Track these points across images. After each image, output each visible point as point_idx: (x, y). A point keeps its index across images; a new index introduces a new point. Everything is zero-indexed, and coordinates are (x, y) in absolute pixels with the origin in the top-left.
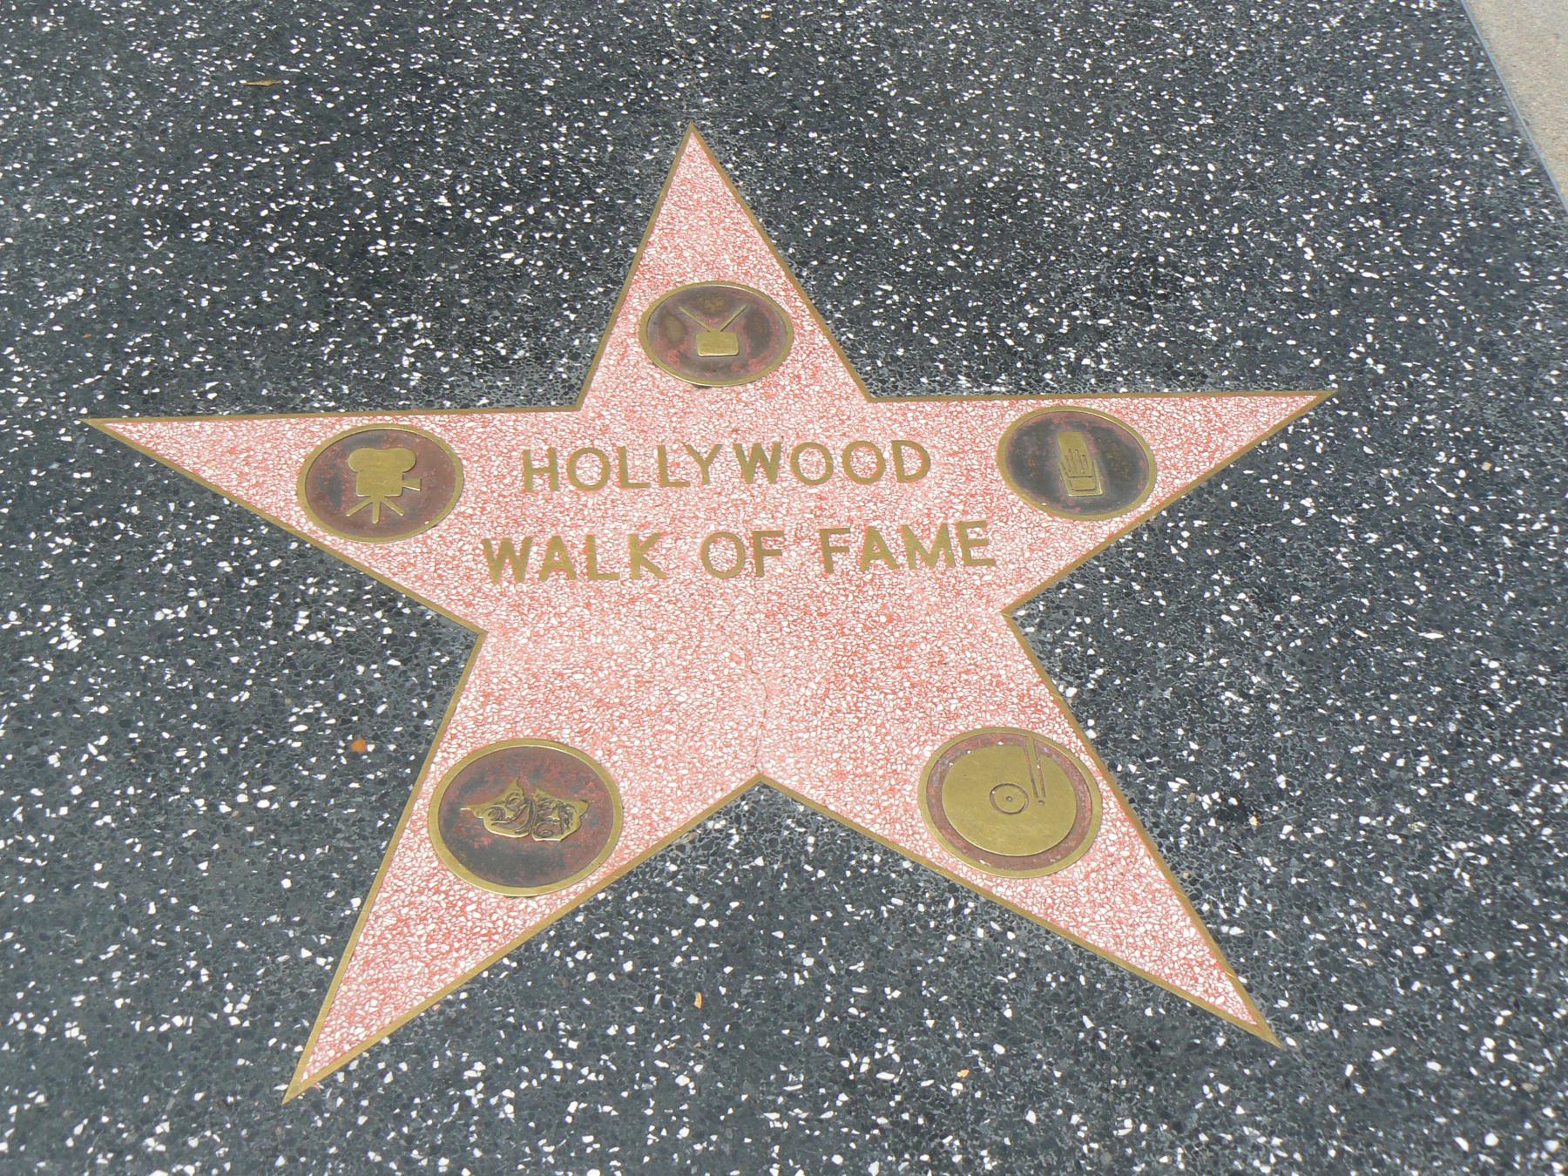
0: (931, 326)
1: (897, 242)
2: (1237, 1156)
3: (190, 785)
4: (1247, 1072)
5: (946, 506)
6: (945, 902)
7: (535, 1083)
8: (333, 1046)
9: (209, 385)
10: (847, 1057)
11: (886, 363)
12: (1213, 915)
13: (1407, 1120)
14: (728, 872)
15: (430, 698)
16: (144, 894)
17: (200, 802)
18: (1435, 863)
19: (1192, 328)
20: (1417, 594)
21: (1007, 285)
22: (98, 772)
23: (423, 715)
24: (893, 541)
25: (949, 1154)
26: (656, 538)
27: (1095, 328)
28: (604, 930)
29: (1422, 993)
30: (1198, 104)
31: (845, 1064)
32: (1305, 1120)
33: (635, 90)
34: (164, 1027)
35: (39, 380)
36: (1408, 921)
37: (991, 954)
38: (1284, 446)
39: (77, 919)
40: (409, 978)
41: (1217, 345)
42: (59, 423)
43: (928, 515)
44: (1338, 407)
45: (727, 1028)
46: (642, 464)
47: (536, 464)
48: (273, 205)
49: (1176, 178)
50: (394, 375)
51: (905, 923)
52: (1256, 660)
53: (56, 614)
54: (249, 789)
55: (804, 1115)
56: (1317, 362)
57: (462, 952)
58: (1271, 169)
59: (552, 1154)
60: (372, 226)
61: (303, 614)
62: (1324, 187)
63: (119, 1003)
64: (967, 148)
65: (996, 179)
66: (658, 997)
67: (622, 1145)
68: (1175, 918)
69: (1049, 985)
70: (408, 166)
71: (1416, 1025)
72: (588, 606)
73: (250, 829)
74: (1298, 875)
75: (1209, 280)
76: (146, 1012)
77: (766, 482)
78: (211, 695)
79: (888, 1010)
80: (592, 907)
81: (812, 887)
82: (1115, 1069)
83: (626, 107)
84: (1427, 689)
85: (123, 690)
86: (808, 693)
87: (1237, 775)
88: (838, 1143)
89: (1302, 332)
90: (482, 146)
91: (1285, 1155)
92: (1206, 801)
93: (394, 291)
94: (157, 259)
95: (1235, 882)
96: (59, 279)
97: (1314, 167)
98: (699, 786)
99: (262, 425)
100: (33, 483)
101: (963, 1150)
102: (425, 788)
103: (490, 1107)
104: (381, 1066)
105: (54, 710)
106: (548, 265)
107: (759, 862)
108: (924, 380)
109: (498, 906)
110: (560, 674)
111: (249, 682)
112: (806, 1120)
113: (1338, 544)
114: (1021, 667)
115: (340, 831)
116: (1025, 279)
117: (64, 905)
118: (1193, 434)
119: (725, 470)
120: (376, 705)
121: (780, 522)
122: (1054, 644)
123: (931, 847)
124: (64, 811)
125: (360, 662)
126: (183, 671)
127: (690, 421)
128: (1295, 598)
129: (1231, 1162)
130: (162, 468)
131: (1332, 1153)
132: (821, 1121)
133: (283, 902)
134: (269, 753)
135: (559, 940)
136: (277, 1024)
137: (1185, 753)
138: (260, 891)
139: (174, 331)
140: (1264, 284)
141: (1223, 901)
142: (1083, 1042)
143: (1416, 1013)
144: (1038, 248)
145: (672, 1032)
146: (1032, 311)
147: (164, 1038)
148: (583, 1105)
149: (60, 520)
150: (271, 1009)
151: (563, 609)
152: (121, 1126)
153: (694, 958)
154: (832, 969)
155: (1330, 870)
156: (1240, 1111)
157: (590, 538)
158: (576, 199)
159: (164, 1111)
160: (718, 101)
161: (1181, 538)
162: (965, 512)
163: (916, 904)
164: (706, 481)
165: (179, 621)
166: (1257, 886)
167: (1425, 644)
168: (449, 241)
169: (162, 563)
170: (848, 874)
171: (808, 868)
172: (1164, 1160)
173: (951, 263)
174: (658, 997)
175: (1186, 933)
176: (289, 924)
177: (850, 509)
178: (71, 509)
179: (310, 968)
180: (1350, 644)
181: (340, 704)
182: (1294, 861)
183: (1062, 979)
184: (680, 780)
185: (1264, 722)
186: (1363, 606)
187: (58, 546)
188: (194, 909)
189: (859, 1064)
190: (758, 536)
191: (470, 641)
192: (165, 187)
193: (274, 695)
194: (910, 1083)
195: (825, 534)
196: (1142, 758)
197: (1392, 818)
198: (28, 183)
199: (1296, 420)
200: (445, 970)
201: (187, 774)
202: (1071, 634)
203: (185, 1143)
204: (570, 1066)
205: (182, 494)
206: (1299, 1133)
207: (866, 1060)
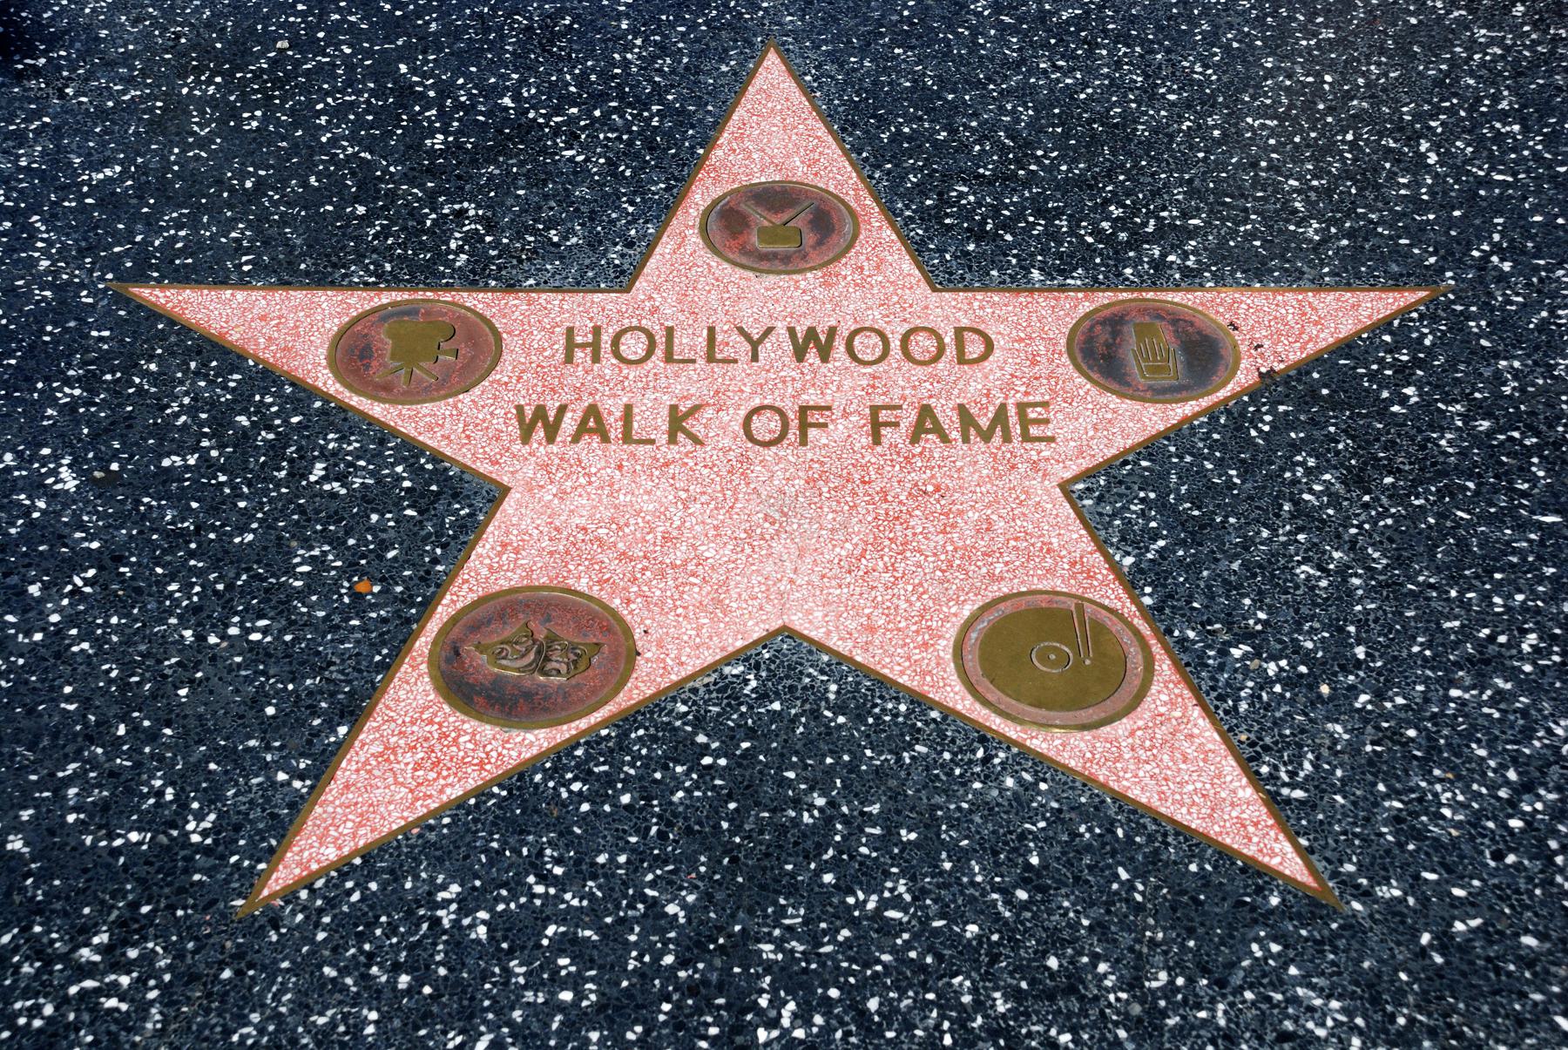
0: (1007, 225)
1: (977, 148)
2: (1288, 1017)
3: (180, 617)
4: (1304, 933)
5: (1008, 387)
6: (974, 752)
7: (513, 905)
8: (299, 864)
9: (244, 259)
10: (854, 894)
11: (955, 257)
12: (1273, 777)
13: (1495, 993)
14: (742, 715)
15: (444, 546)
16: (115, 716)
17: (188, 633)
18: (1540, 739)
19: (1292, 228)
20: (1534, 480)
21: (1090, 187)
22: (80, 602)
23: (435, 561)
24: (948, 418)
25: (958, 994)
26: (696, 409)
27: (1185, 228)
28: (604, 764)
29: (1518, 866)
30: (1320, 20)
31: (851, 900)
32: (1370, 986)
33: (716, 8)
34: (118, 842)
35: (64, 247)
36: (1503, 793)
37: (1021, 802)
38: (1387, 338)
39: (37, 738)
40: (390, 803)
41: (1319, 243)
42: (82, 286)
43: (987, 396)
44: (1453, 302)
45: (726, 861)
46: (690, 341)
47: (579, 340)
48: (330, 100)
49: (1287, 89)
50: (440, 257)
51: (927, 769)
52: (1339, 536)
53: (56, 458)
54: (242, 623)
55: (801, 948)
56: (1432, 260)
57: (450, 780)
58: (1396, 79)
59: (524, 975)
60: (431, 122)
61: (319, 466)
62: (1455, 95)
63: (71, 818)
64: (1061, 63)
65: (1089, 91)
66: (654, 829)
67: (601, 968)
68: (1229, 778)
69: (1082, 835)
70: (473, 69)
71: (1509, 898)
72: (620, 467)
73: (238, 659)
74: (1373, 743)
75: (1315, 183)
76: (100, 827)
77: (818, 361)
78: (212, 536)
79: (902, 851)
80: (594, 742)
81: (829, 731)
82: (1151, 921)
83: (705, 23)
84: (1539, 569)
85: (118, 528)
86: (844, 553)
87: (1309, 645)
88: (835, 976)
89: (1418, 233)
90: (552, 54)
91: (1344, 1019)
92: (1272, 669)
93: (448, 181)
94: (203, 143)
95: (1300, 746)
96: (95, 157)
97: (1447, 76)
98: (719, 635)
99: (298, 296)
100: (47, 339)
101: (974, 991)
102: (429, 626)
103: (461, 928)
104: (349, 884)
105: (42, 543)
106: (609, 162)
107: (776, 706)
108: (994, 273)
109: (494, 738)
110: (584, 529)
111: (255, 526)
112: (803, 953)
113: (1442, 430)
114: (1075, 536)
115: (334, 664)
116: (1111, 182)
117: (25, 723)
118: (1282, 325)
119: (777, 349)
120: (387, 550)
121: (829, 398)
122: (1114, 516)
123: (963, 699)
124: (38, 637)
125: (374, 511)
126: (185, 513)
127: (743, 305)
128: (1388, 480)
129: (1281, 1022)
130: (186, 330)
131: (1401, 1021)
132: (819, 955)
133: (267, 729)
134: (267, 591)
135: (556, 771)
136: (242, 842)
137: (1251, 622)
138: (242, 717)
139: (214, 209)
140: (1377, 187)
141: (1285, 764)
142: (1116, 893)
143: (1509, 886)
144: (1129, 154)
145: (666, 862)
146: (1116, 211)
147: (116, 852)
148: (562, 929)
149: (71, 373)
150: (237, 828)
151: (593, 470)
152: (54, 936)
153: (697, 794)
154: (845, 809)
155: (1412, 740)
156: (1293, 971)
157: (628, 409)
158: (645, 104)
159: (104, 923)
160: (802, 19)
161: (1263, 421)
162: (1027, 394)
163: (941, 752)
164: (755, 358)
165: (187, 468)
166: (1325, 752)
167: (1540, 526)
168: (509, 138)
169: (177, 415)
170: (871, 720)
171: (828, 713)
172: (1203, 1014)
173: (1033, 167)
174: (654, 829)
175: (1241, 793)
176: (268, 748)
177: (903, 388)
178: (84, 363)
179: (285, 790)
180: (1449, 524)
181: (349, 548)
182: (1369, 729)
183: (1098, 831)
184: (699, 628)
185: (1343, 595)
186: (1468, 489)
187: (66, 395)
188: (168, 731)
189: (865, 902)
190: (804, 410)
191: (495, 495)
192: (218, 80)
193: (280, 538)
194: (920, 922)
195: (875, 410)
196: (1203, 625)
197: (1489, 692)
198: (73, 70)
199: (1403, 313)
200: (430, 796)
201: (178, 606)
202: (1133, 508)
203: (124, 954)
204: (552, 891)
205: (205, 354)
206: (1361, 998)
207: (874, 897)
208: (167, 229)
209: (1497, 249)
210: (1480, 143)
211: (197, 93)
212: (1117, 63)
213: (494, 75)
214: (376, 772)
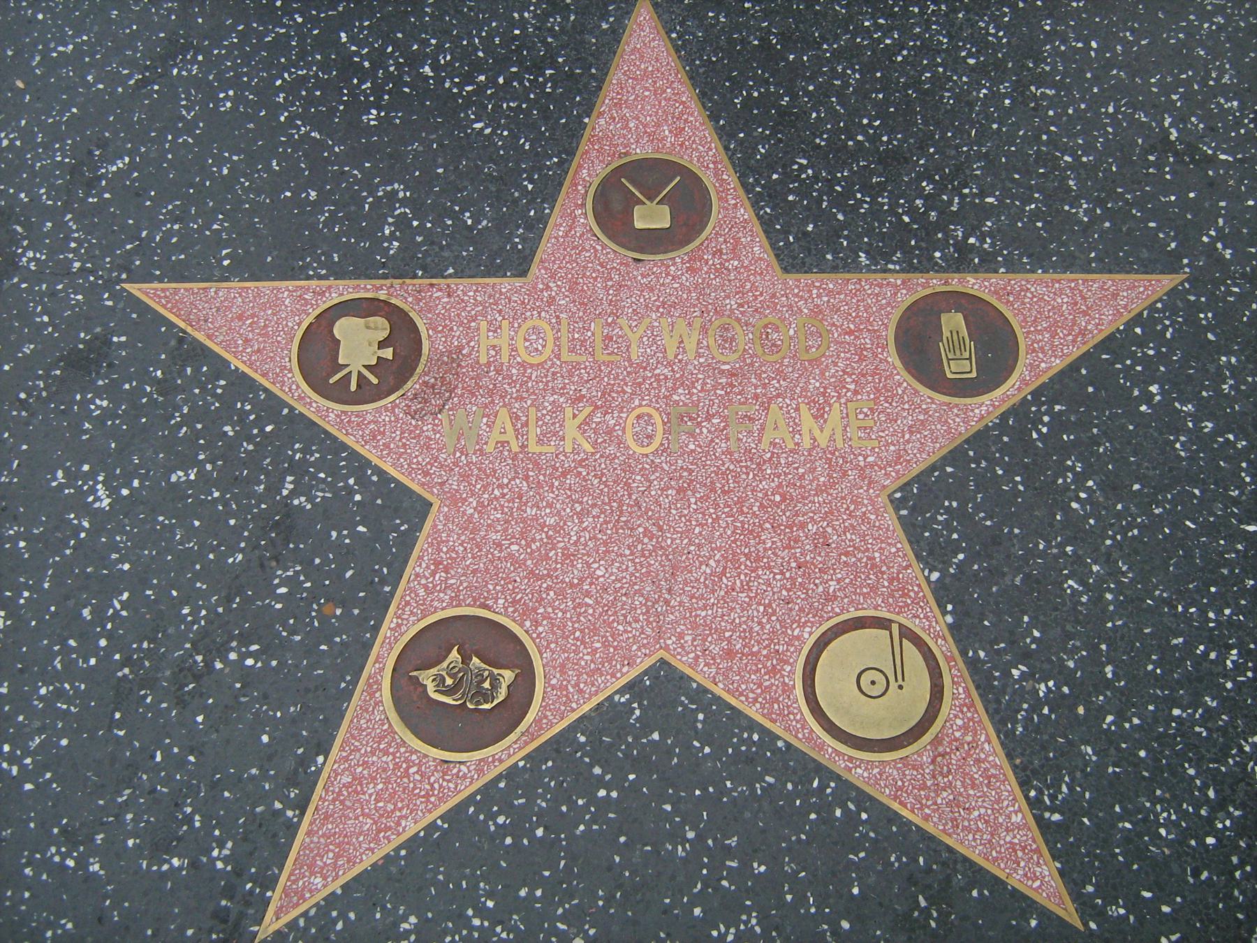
17: (199, 658)
43: (824, 394)
53: (92, 475)
68: (1006, 803)
69: (893, 864)
72: (526, 478)
94: (190, 128)
144: (937, 124)
147: (163, 876)
166: (1078, 775)
169: (179, 426)
173: (860, 138)
182: (1112, 751)
198: (92, 56)
207: (732, 930)
208: (164, 223)
209: (1221, 236)
210: (1207, 117)
211: (184, 73)
212: (928, 21)
213: (416, 41)
214: (348, 803)
